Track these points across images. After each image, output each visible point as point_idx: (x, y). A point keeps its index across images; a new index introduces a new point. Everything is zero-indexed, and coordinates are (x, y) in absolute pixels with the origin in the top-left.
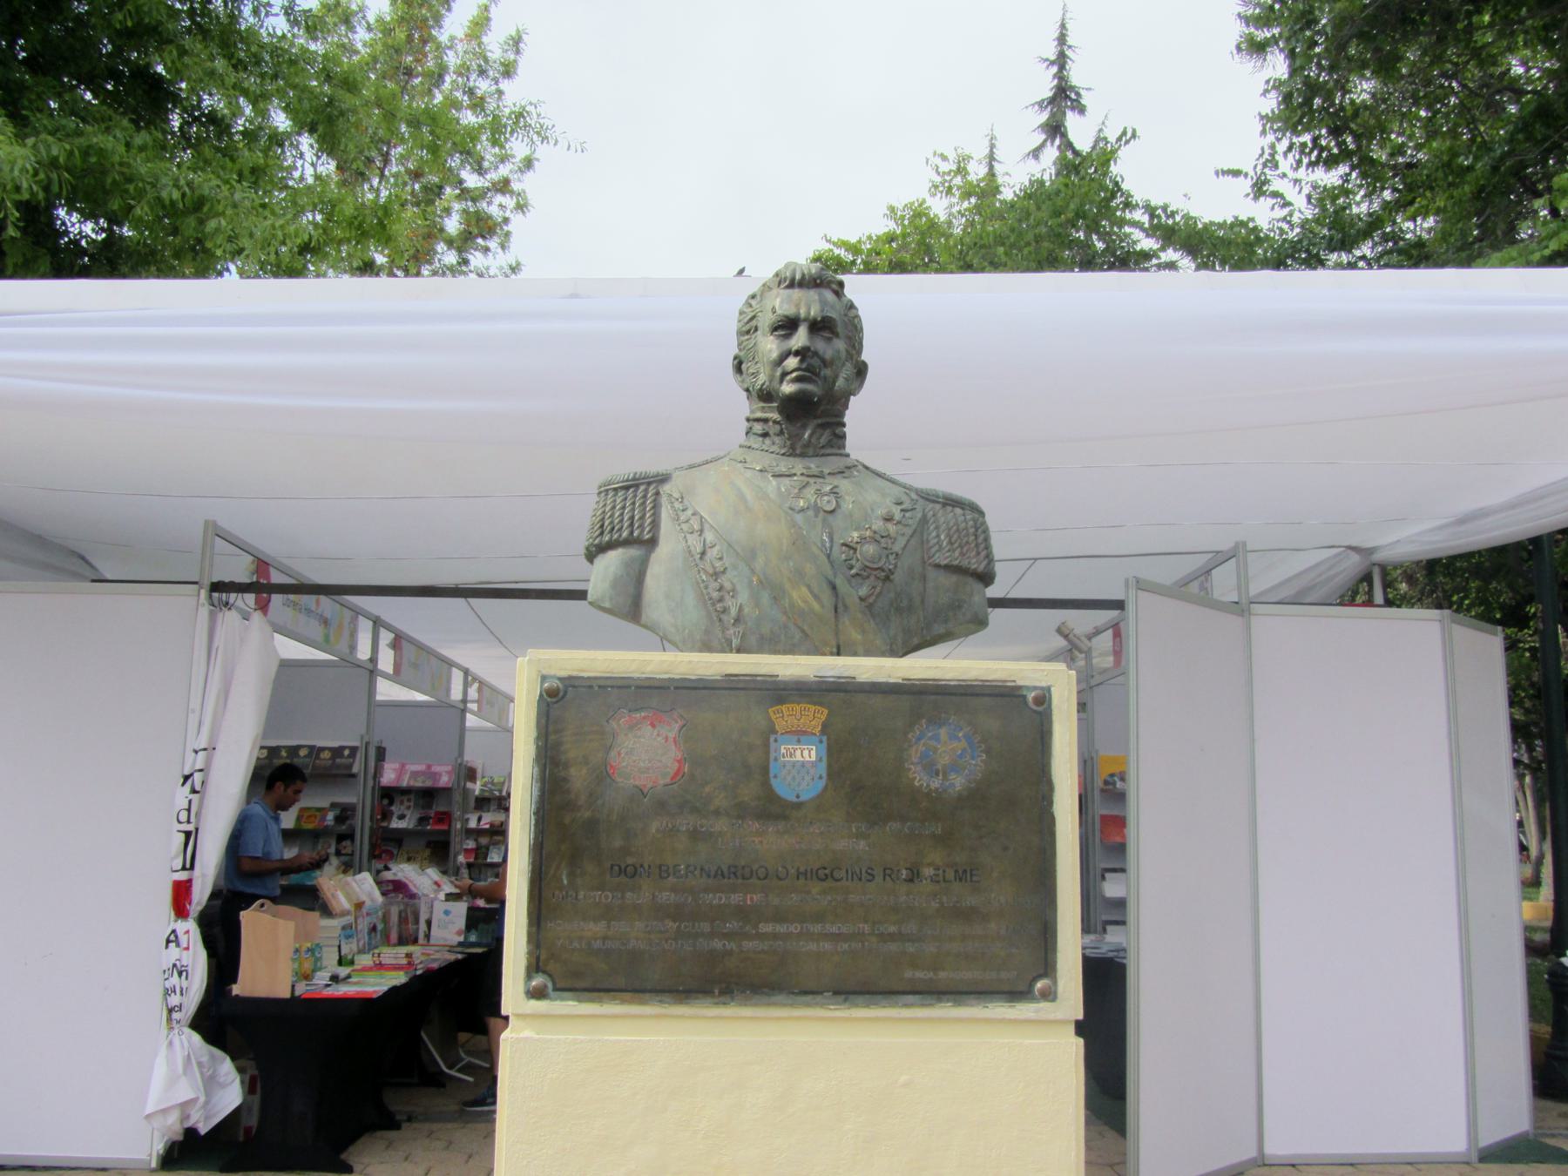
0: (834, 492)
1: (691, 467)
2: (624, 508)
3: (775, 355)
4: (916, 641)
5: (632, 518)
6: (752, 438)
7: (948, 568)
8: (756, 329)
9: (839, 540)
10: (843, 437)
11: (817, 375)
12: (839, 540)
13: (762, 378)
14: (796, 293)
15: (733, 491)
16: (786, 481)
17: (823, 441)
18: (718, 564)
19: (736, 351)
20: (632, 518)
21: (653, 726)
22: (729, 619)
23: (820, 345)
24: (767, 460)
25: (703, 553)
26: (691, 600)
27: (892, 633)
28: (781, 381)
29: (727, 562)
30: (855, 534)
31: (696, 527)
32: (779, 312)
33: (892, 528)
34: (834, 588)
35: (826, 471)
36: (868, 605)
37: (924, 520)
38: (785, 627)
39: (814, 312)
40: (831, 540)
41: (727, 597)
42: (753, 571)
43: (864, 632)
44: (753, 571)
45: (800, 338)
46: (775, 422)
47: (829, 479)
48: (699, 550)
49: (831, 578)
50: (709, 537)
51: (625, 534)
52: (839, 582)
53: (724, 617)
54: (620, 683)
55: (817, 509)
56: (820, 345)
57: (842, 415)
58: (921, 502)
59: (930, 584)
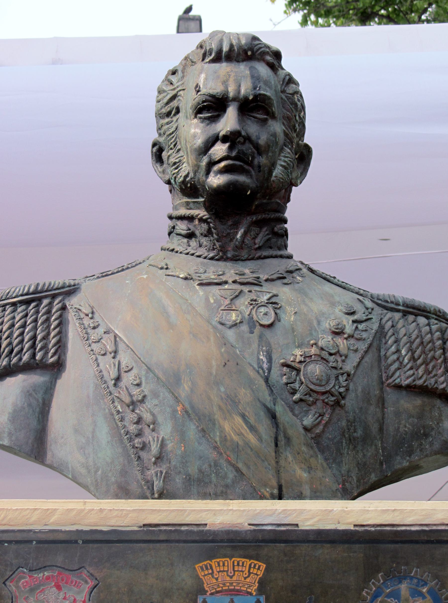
0: (272, 302)
1: (105, 275)
2: (24, 326)
3: (199, 142)
4: (373, 478)
5: (34, 338)
6: (176, 239)
7: (411, 389)
8: (178, 111)
9: (278, 360)
10: (285, 234)
11: (251, 164)
12: (278, 360)
13: (186, 169)
14: (224, 68)
15: (157, 311)
16: (215, 289)
17: (259, 241)
18: (135, 391)
19: (154, 136)
20: (34, 338)
21: (59, 588)
22: (148, 457)
23: (253, 129)
24: (192, 266)
25: (118, 379)
26: (104, 433)
27: (344, 468)
28: (208, 172)
29: (146, 389)
30: (298, 352)
31: (110, 348)
32: (203, 91)
33: (342, 343)
34: (273, 416)
35: (263, 277)
36: (316, 438)
37: (381, 333)
38: (216, 464)
39: (246, 89)
40: (270, 360)
41: (147, 431)
42: (177, 399)
43: (310, 469)
44: (177, 399)
45: (229, 121)
46: (201, 220)
47: (266, 287)
48: (114, 374)
49: (270, 405)
50: (125, 358)
51: (26, 357)
52: (279, 409)
53: (143, 454)
54: (19, 537)
55: (253, 323)
56: (253, 129)
57: (282, 209)
58: (378, 310)
59: (390, 410)
